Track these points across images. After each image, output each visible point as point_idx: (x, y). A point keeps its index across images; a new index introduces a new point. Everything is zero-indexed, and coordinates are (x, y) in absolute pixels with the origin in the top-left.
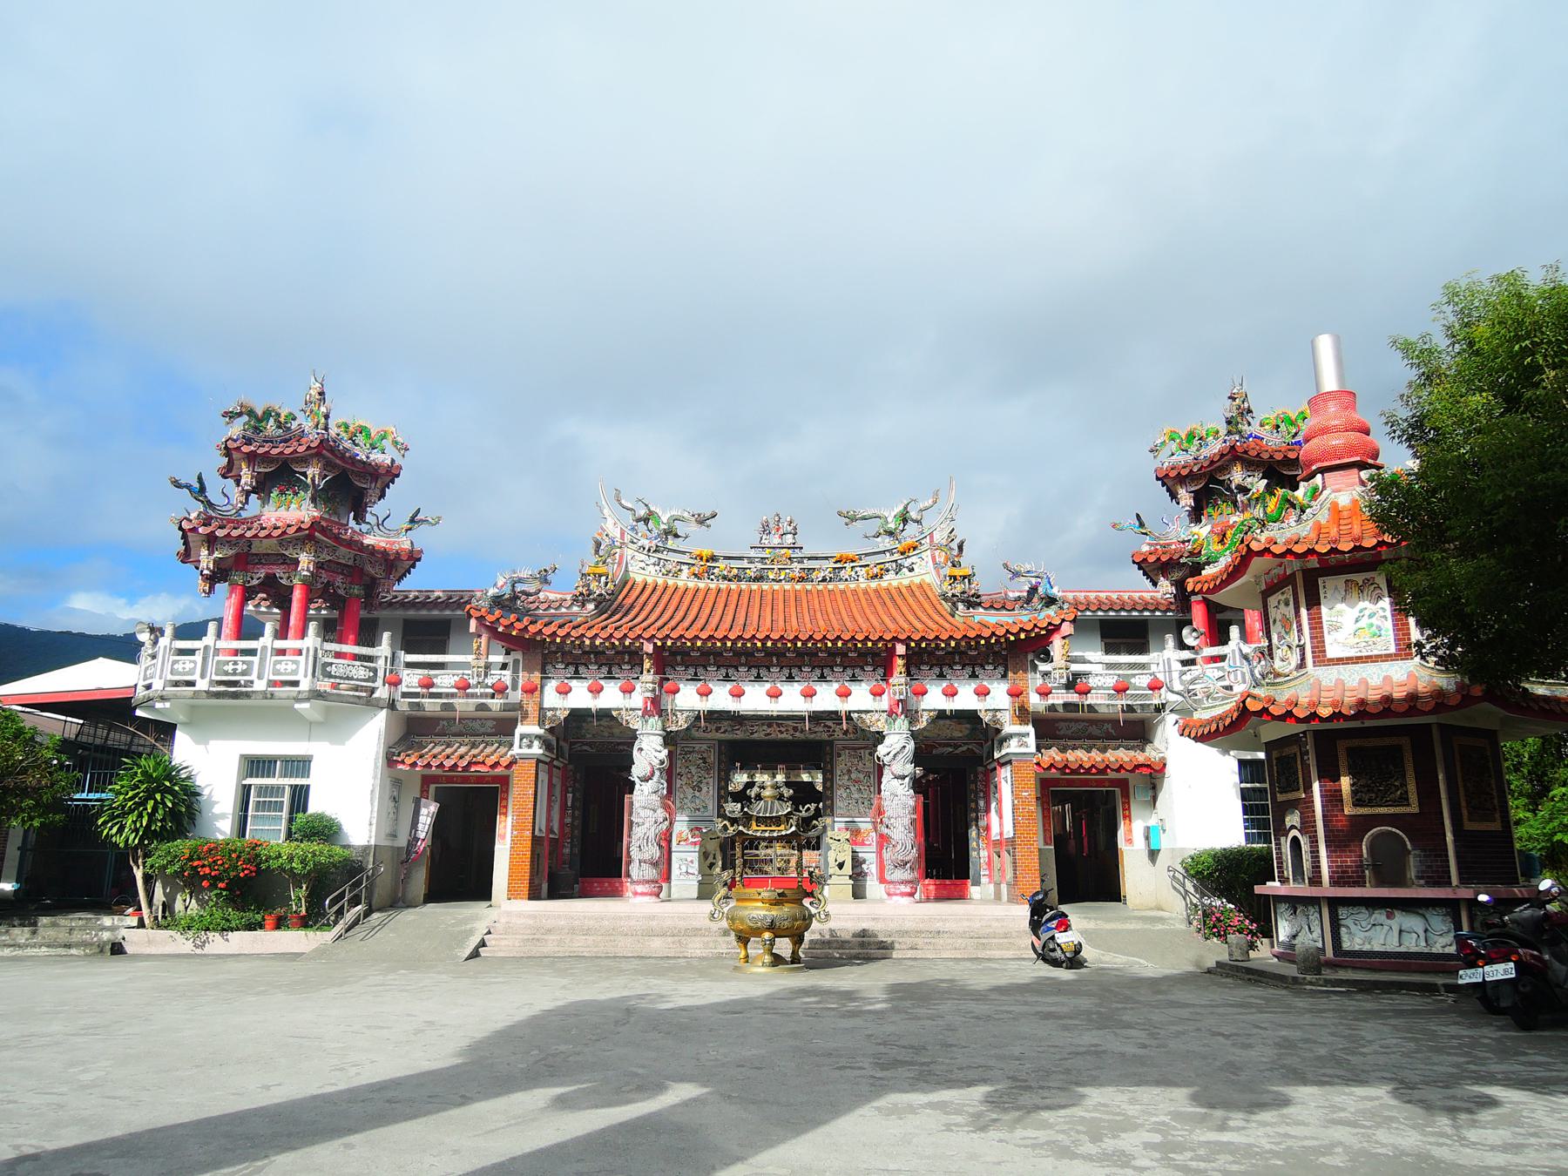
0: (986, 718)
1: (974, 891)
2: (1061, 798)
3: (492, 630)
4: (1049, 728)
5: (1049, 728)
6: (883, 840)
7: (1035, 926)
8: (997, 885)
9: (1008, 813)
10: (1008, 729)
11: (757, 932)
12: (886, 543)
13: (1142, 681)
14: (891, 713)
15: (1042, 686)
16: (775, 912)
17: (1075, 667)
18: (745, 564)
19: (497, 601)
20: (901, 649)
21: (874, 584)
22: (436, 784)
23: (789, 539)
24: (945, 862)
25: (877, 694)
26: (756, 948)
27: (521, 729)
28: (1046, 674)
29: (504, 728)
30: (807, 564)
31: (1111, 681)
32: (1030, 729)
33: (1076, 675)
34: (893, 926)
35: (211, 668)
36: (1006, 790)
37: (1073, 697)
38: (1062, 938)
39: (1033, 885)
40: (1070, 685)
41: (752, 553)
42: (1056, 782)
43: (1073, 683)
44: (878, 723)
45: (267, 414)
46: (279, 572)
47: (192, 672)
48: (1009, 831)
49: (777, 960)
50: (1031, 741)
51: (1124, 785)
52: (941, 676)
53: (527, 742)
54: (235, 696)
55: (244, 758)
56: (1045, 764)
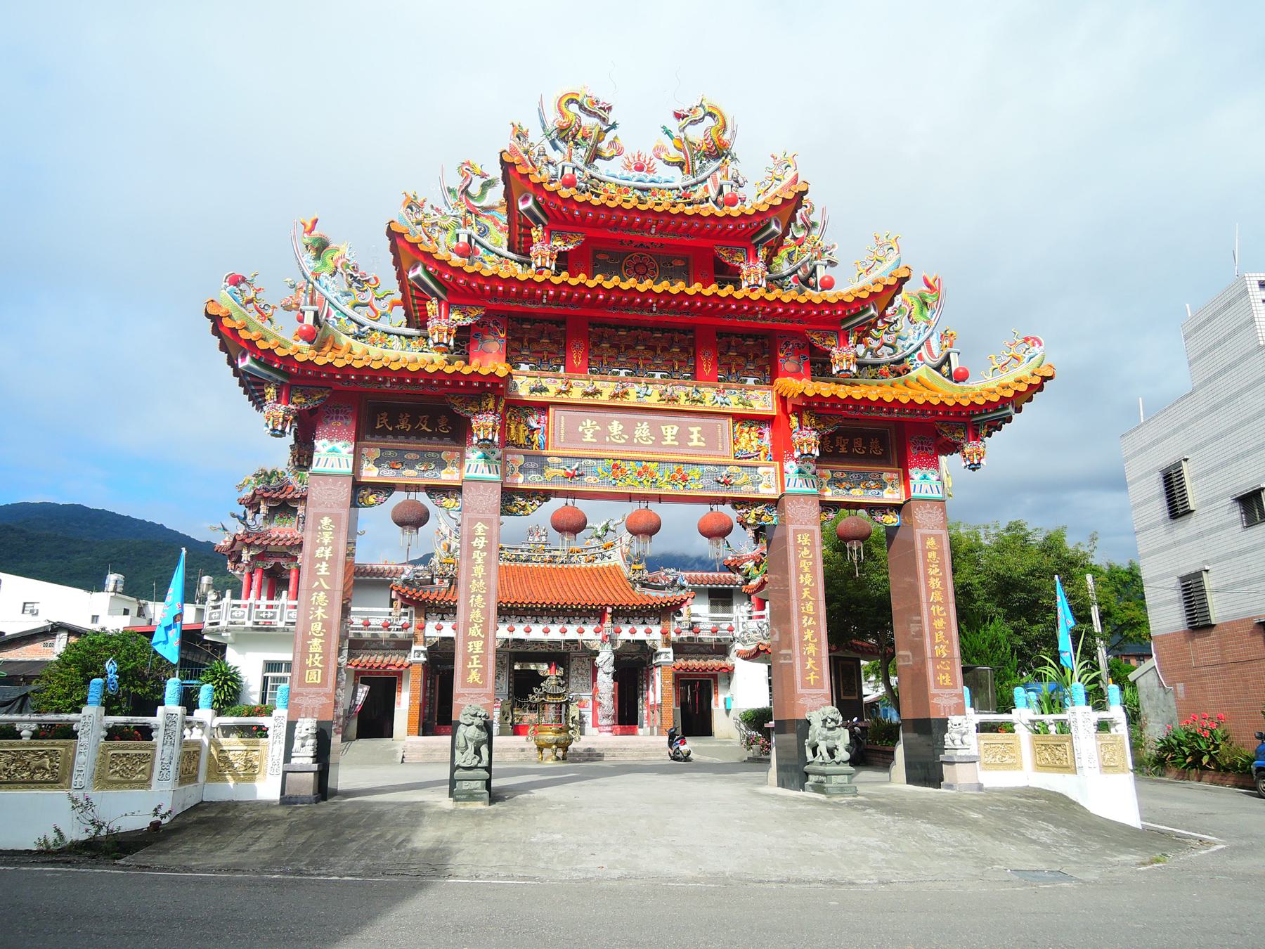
0: (650, 644)
1: (640, 731)
2: (685, 683)
3: (403, 597)
4: (680, 649)
5: (680, 649)
6: (597, 705)
7: (670, 744)
8: (652, 728)
9: (658, 692)
10: (660, 650)
11: (549, 746)
12: (596, 542)
13: (725, 626)
14: (603, 641)
15: (677, 629)
16: (558, 736)
17: (693, 619)
18: (519, 552)
19: (406, 582)
20: (609, 610)
21: (589, 565)
22: (362, 677)
23: (544, 539)
24: (627, 716)
25: (597, 632)
26: (547, 752)
27: (414, 648)
28: (679, 622)
29: (405, 646)
30: (553, 553)
31: (710, 627)
32: (671, 650)
33: (694, 623)
34: (602, 746)
35: (253, 615)
36: (658, 680)
37: (691, 634)
38: (682, 748)
39: (669, 725)
40: (691, 629)
41: (523, 546)
42: (682, 675)
43: (693, 626)
44: (596, 646)
45: (273, 473)
46: (282, 562)
47: (242, 617)
48: (659, 700)
49: (558, 759)
50: (671, 655)
51: (715, 677)
52: (628, 623)
53: (417, 655)
54: (268, 630)
55: (1105, 710)
56: (678, 667)
